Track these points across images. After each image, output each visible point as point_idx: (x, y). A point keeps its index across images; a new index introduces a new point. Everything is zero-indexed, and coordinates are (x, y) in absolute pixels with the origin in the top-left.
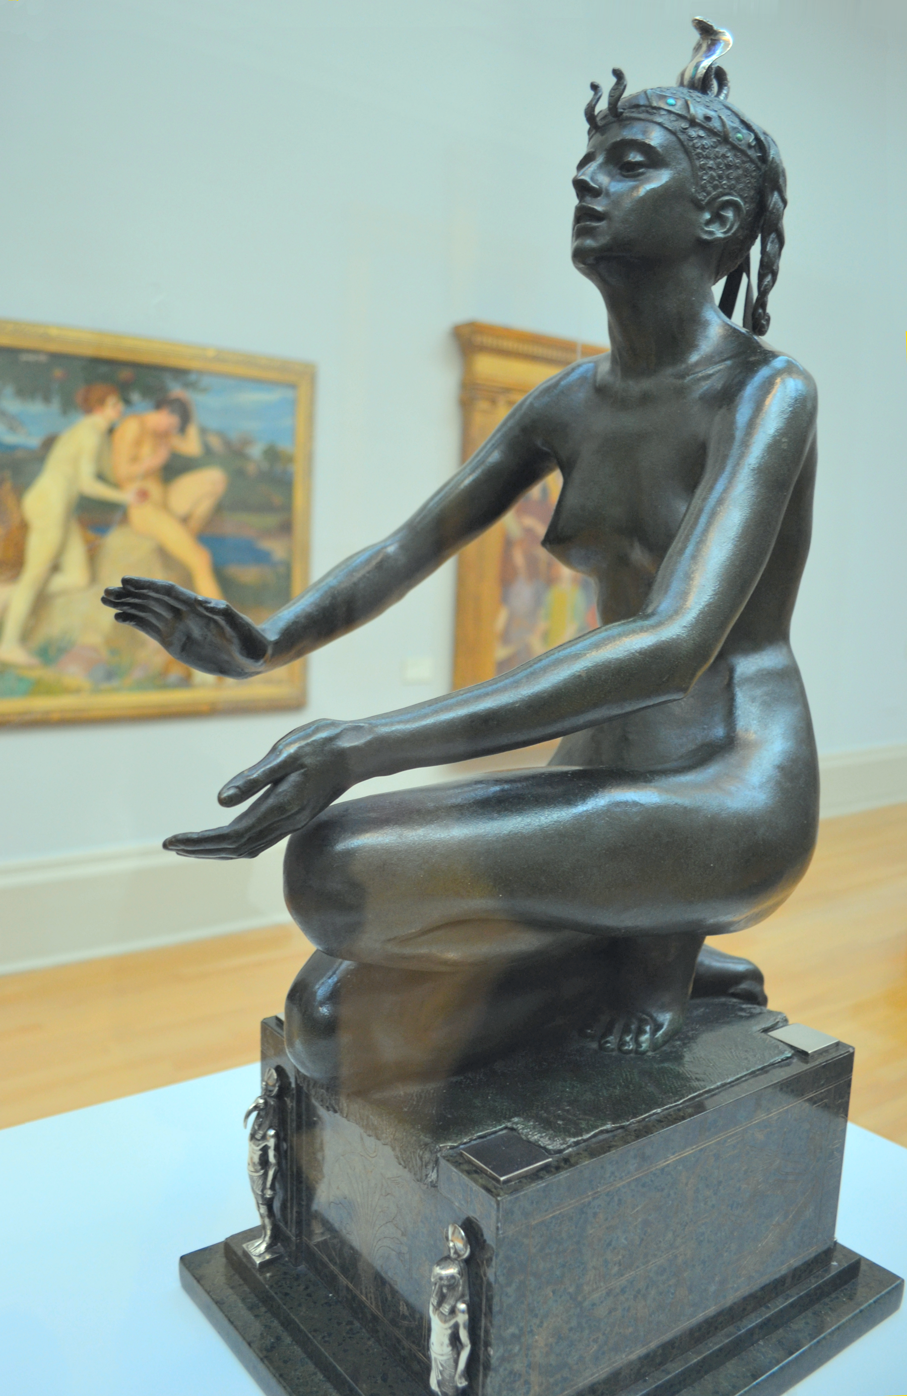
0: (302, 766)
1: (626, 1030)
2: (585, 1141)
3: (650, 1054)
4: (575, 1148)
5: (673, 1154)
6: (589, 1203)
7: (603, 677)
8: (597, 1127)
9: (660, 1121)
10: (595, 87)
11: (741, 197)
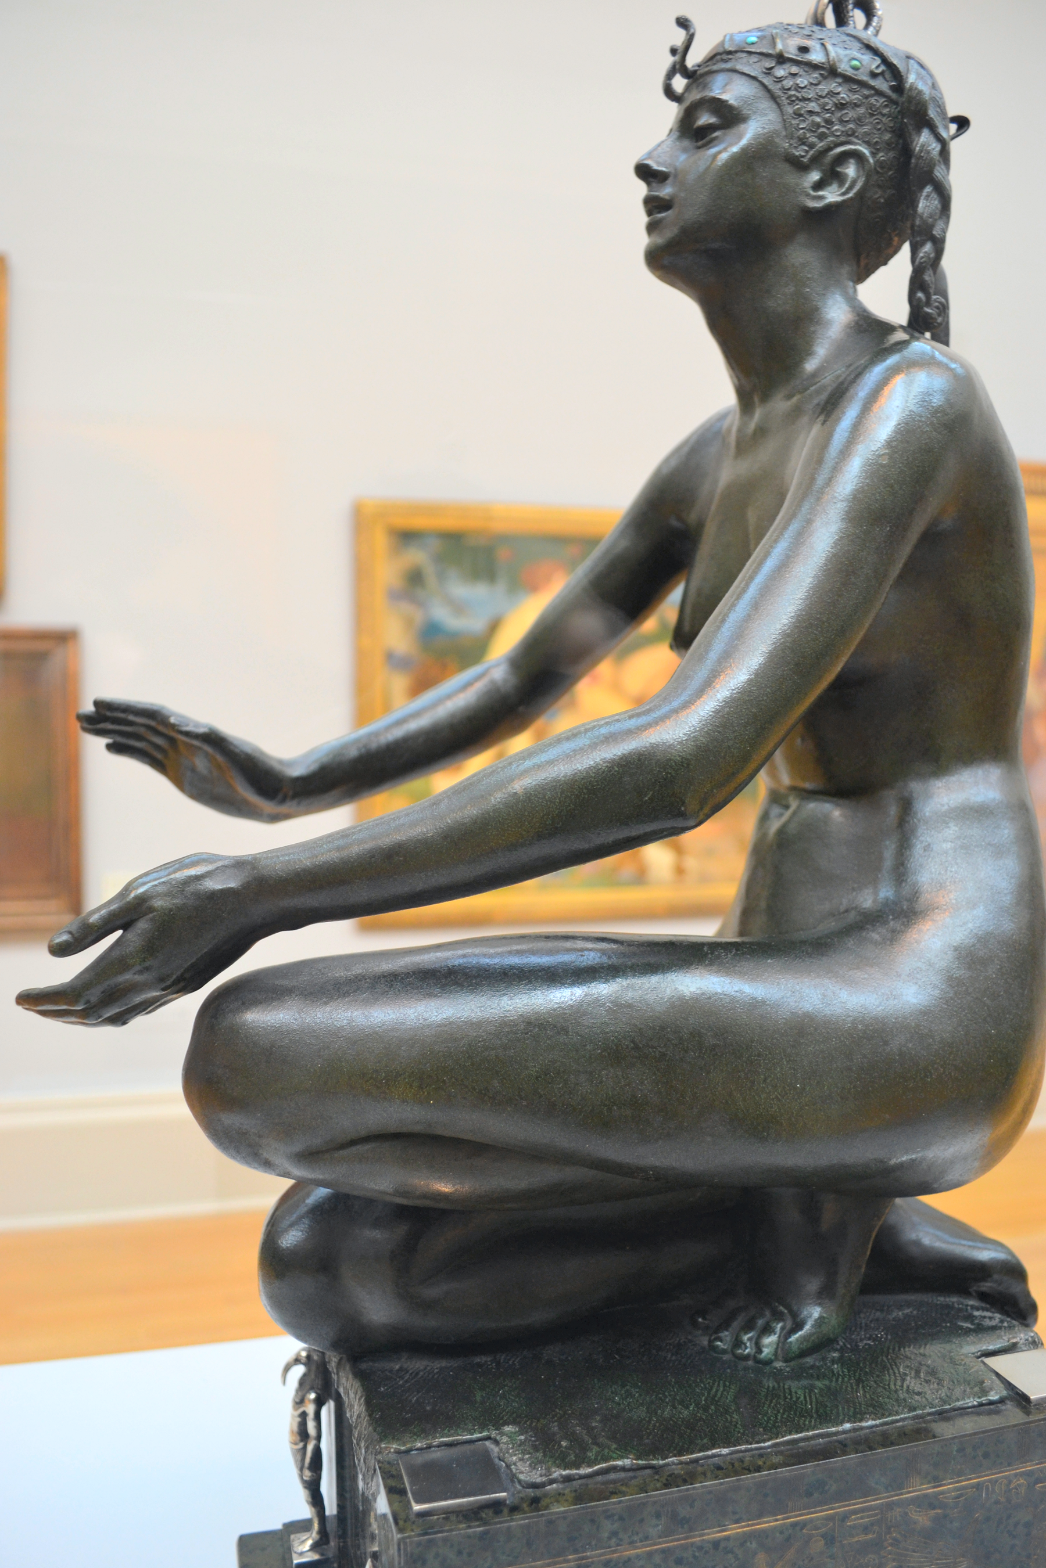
0: (151, 909)
1: (749, 1326)
2: (582, 1477)
3: (778, 1364)
4: (561, 1486)
5: (737, 1522)
8: (606, 1460)
11: (868, 143)
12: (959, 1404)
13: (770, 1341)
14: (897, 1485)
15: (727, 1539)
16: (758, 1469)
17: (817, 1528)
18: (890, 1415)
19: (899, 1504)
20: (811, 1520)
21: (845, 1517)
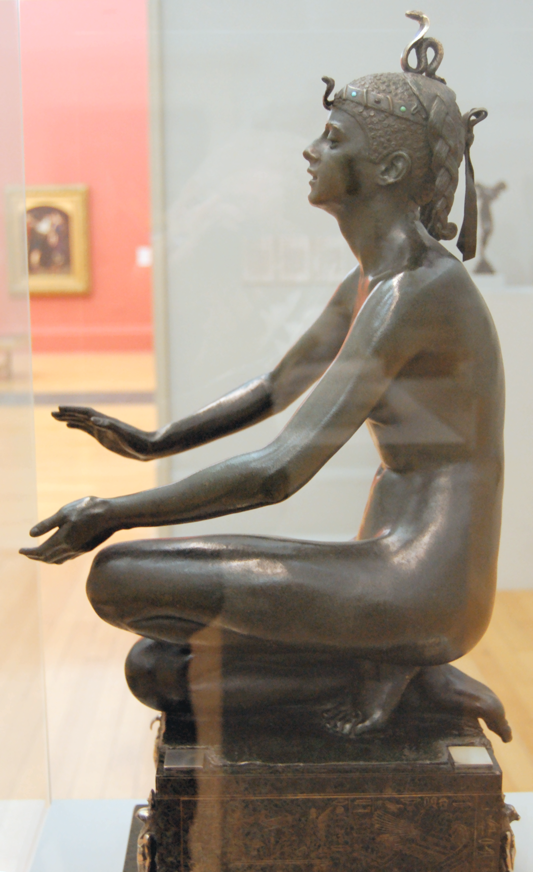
13: (348, 726)
15: (297, 799)
17: (339, 802)
19: (381, 799)
20: (336, 799)
21: (354, 800)
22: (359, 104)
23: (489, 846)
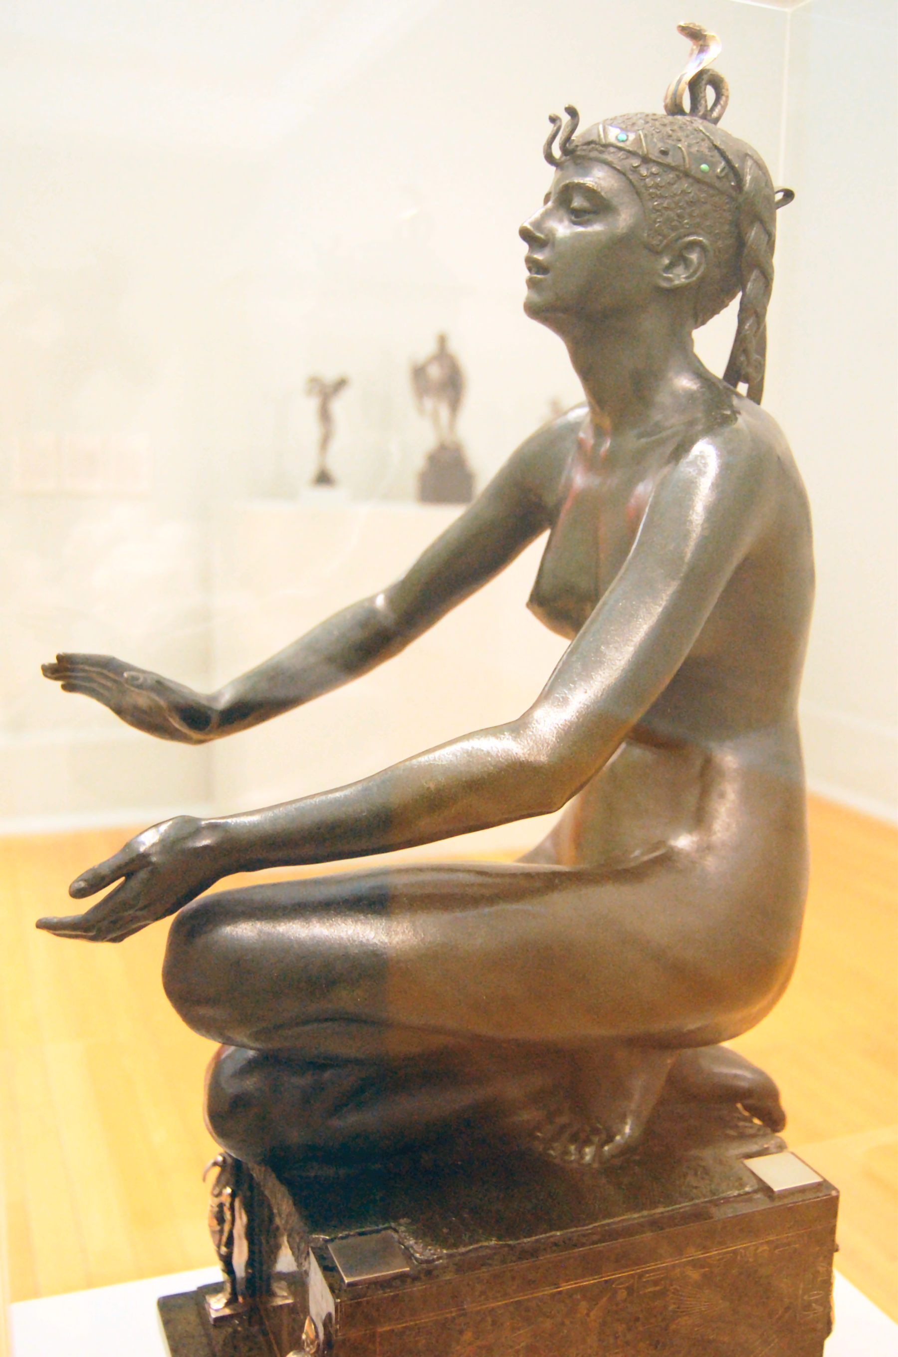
0: (150, 863)
6: (454, 1318)
7: (453, 790)
9: (556, 1244)
10: (553, 120)
12: (724, 1195)
13: (589, 1152)
14: (679, 1251)
16: (583, 1245)
17: (622, 1283)
18: (676, 1204)
21: (641, 1276)
22: (632, 153)
23: (816, 1301)
